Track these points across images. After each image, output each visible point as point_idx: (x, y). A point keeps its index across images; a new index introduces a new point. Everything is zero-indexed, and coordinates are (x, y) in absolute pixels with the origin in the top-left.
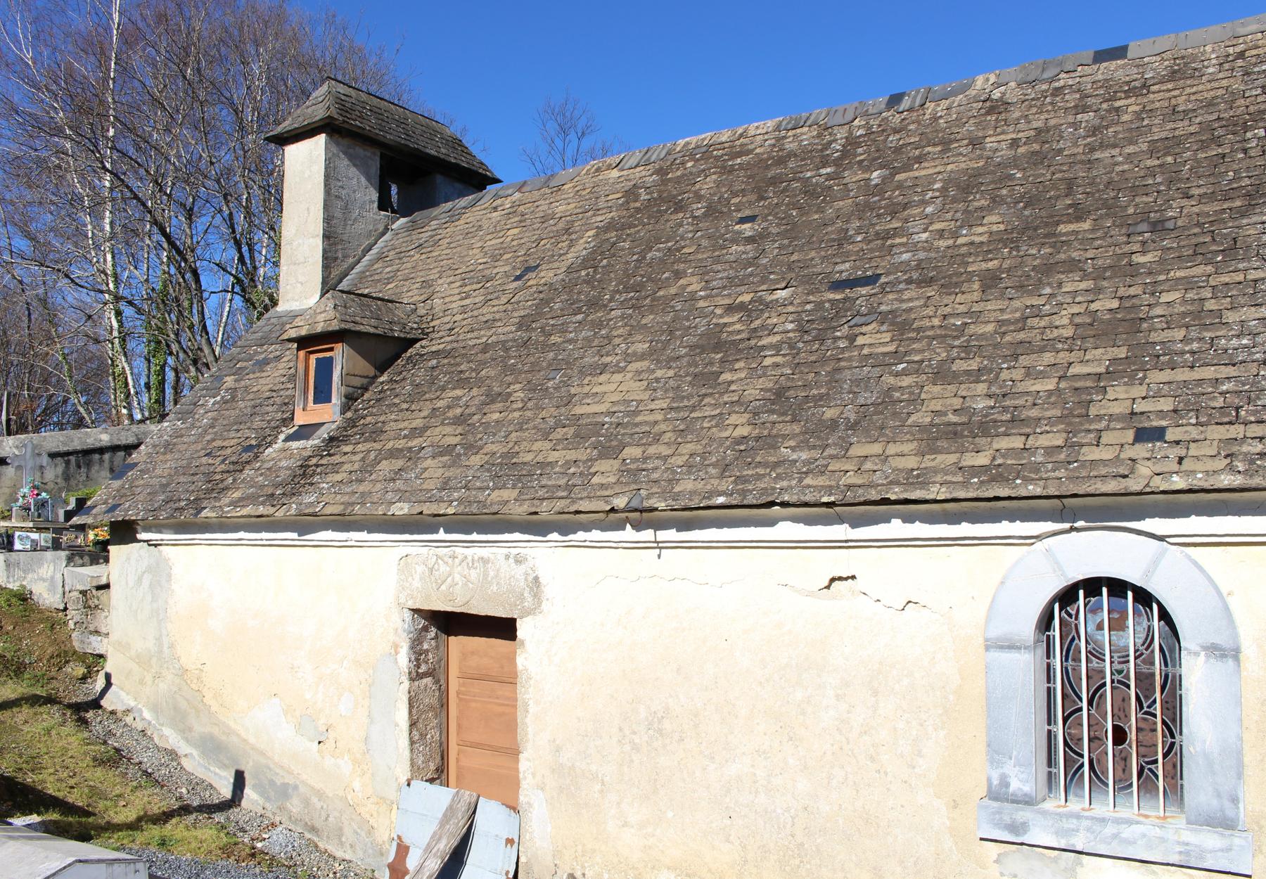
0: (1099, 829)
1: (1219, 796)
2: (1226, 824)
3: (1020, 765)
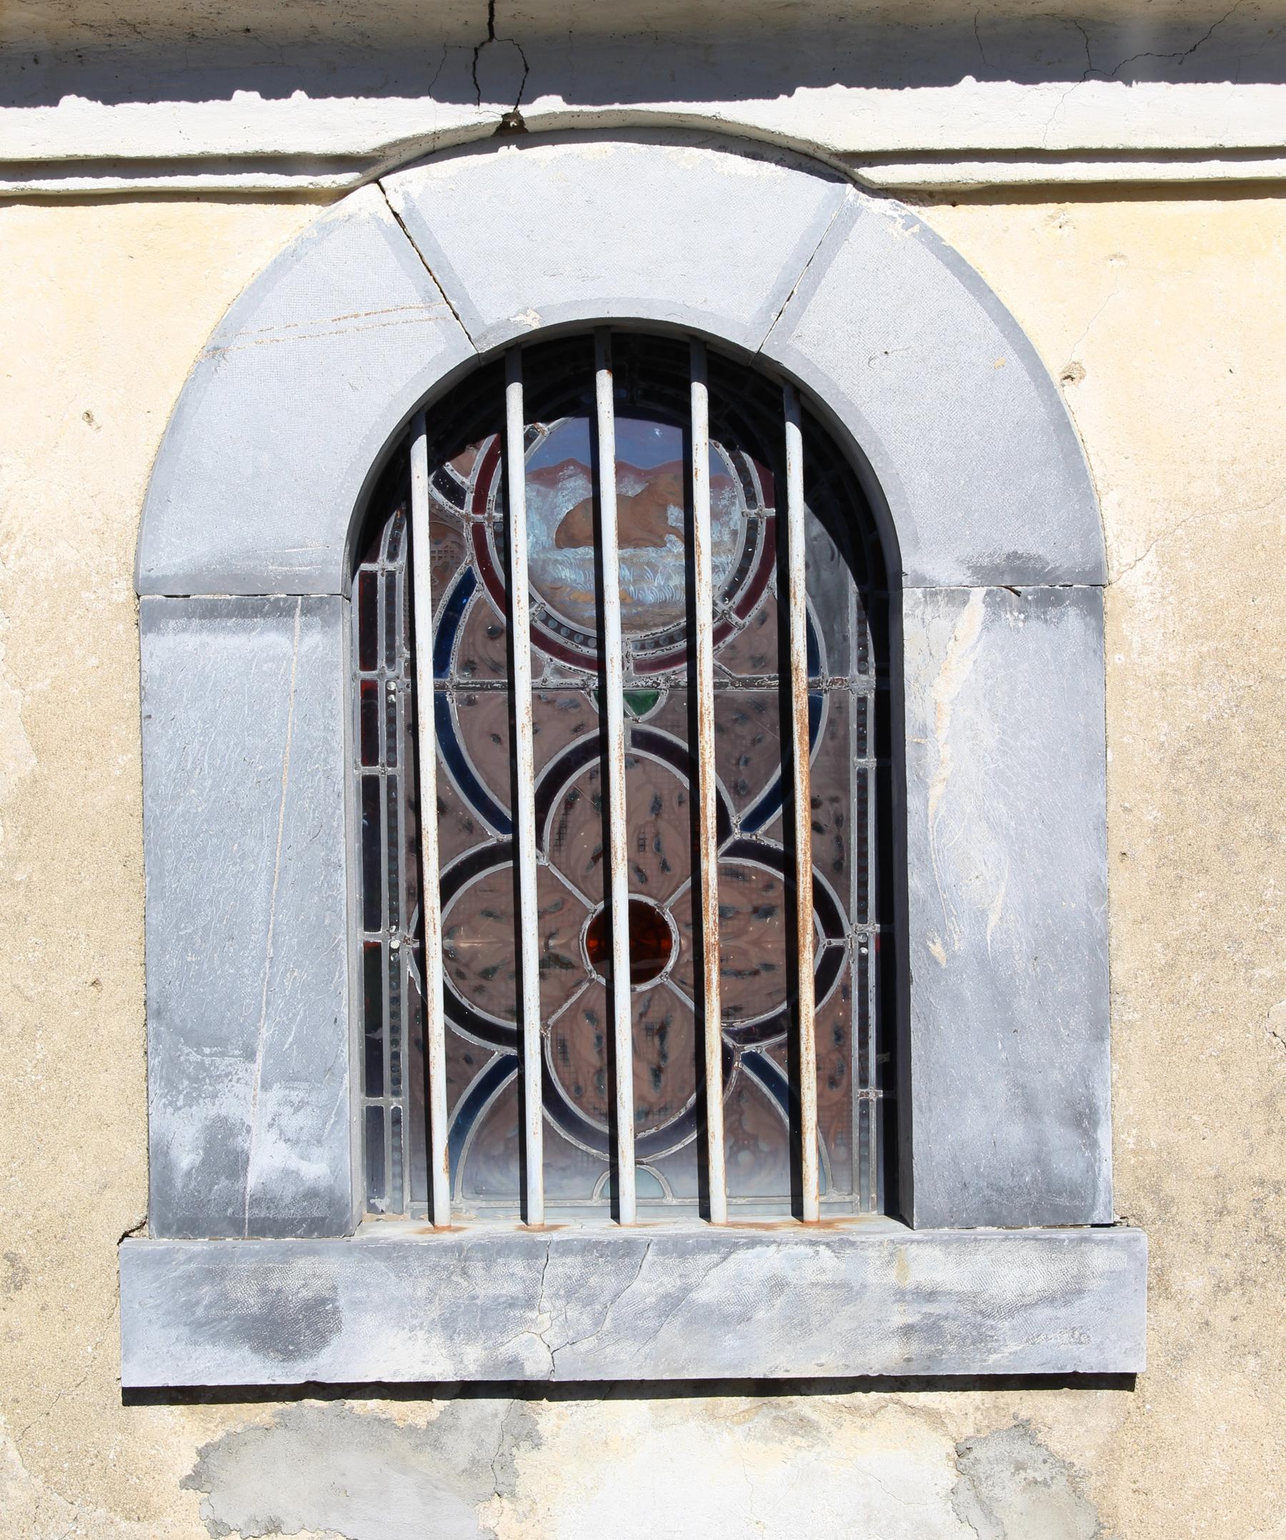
0: (611, 1283)
1: (1029, 1108)
2: (1051, 1207)
3: (291, 1079)
